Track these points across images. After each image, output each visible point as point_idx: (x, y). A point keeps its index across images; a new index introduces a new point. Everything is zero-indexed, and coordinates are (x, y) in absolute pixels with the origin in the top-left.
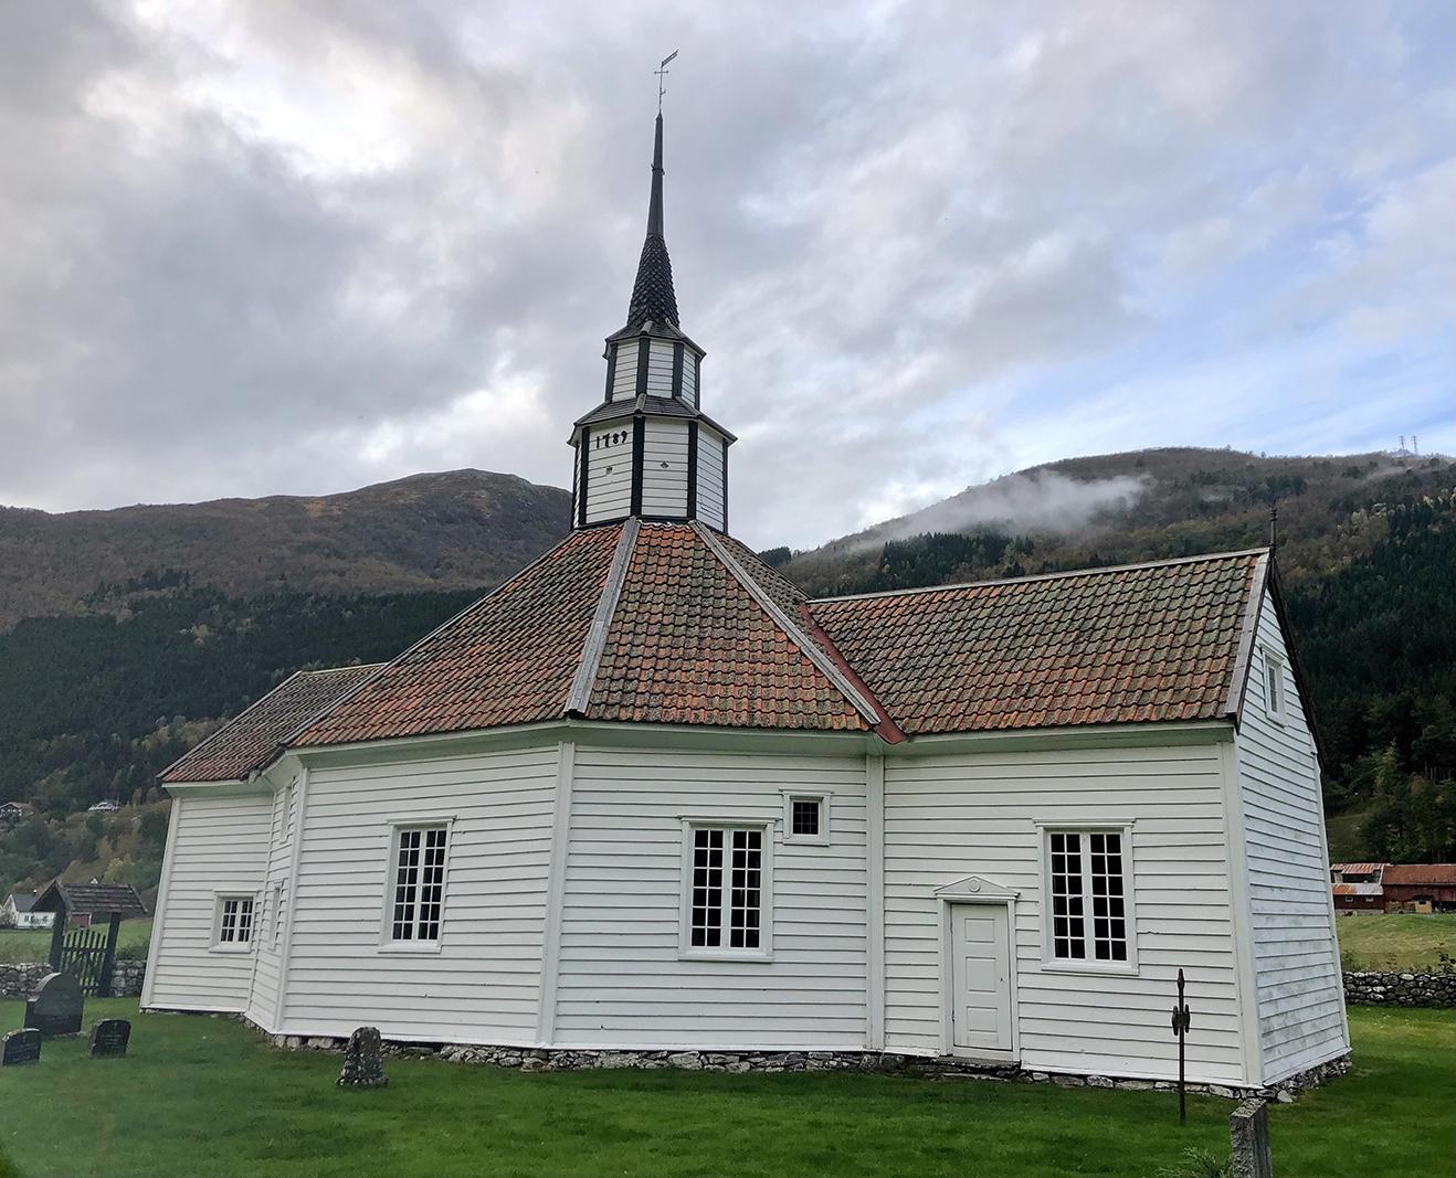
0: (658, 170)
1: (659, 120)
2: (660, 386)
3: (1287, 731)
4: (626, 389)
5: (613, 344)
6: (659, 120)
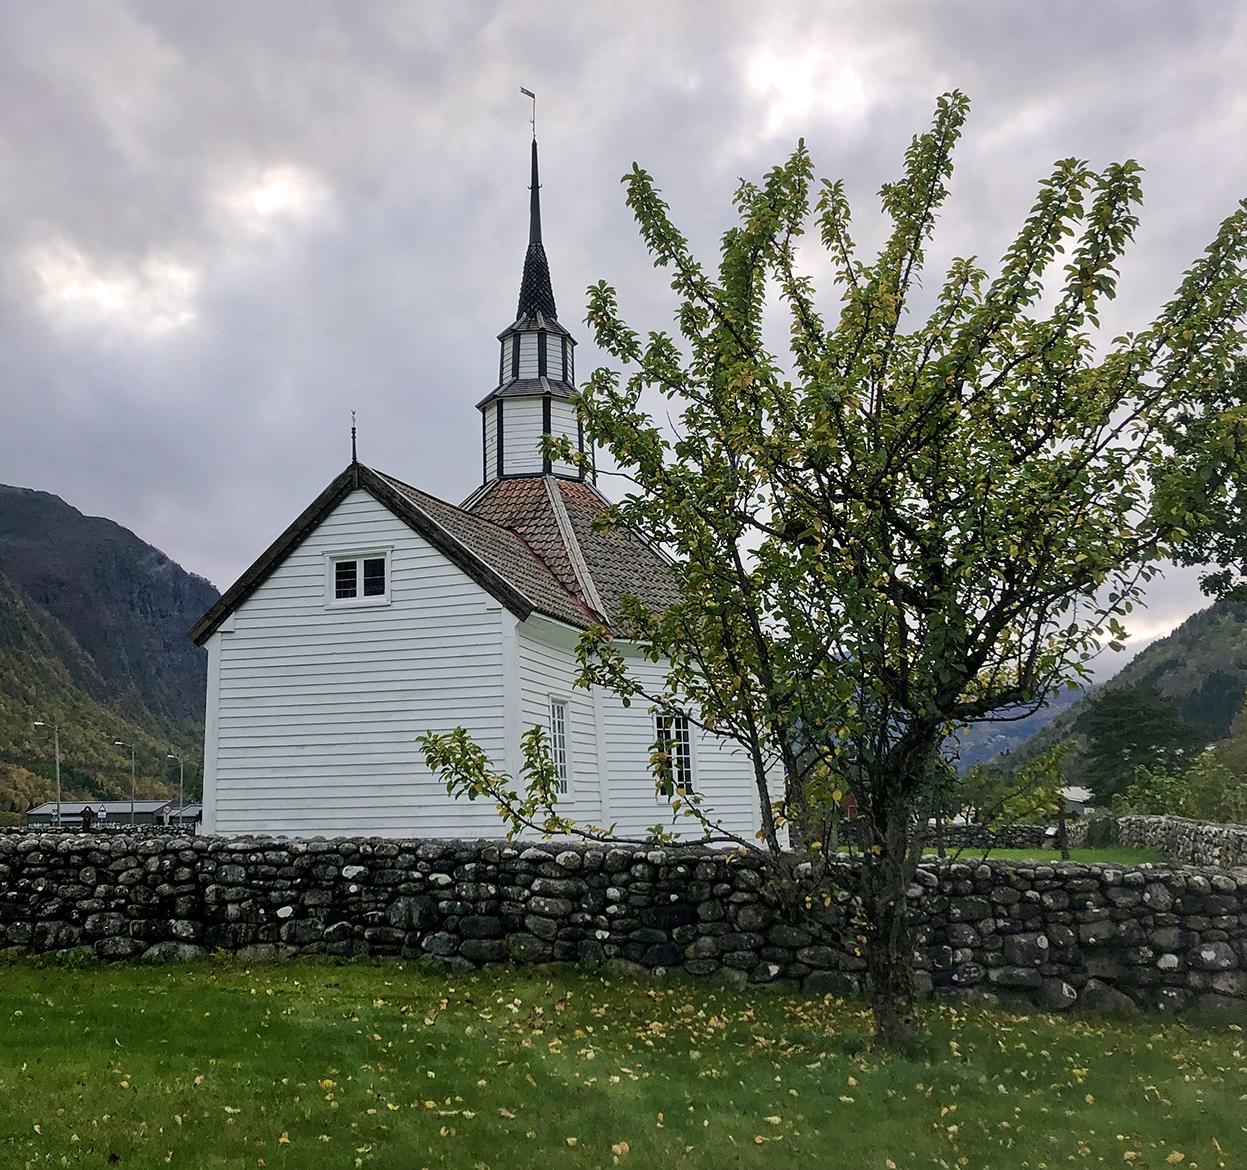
0: (535, 187)
1: (534, 144)
2: (554, 371)
3: (395, 606)
4: (529, 370)
5: (512, 335)
6: (534, 144)
